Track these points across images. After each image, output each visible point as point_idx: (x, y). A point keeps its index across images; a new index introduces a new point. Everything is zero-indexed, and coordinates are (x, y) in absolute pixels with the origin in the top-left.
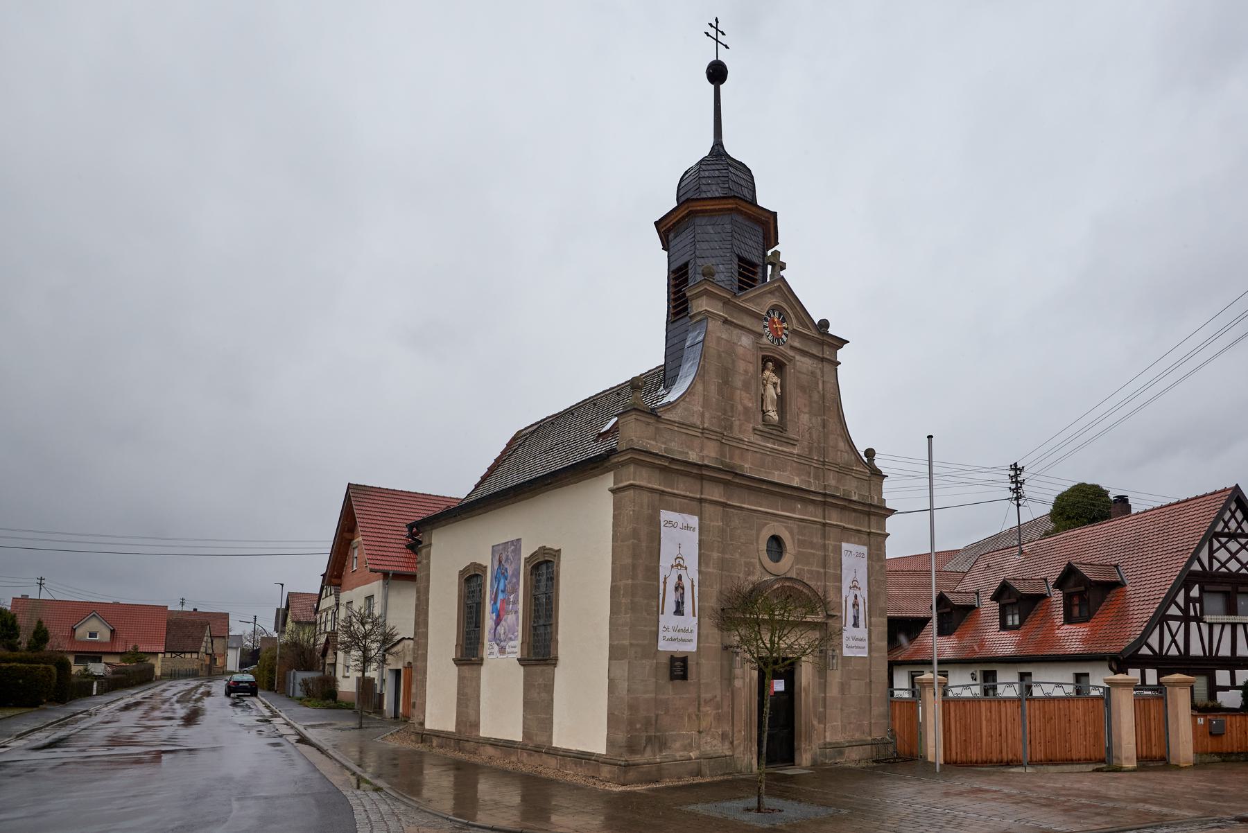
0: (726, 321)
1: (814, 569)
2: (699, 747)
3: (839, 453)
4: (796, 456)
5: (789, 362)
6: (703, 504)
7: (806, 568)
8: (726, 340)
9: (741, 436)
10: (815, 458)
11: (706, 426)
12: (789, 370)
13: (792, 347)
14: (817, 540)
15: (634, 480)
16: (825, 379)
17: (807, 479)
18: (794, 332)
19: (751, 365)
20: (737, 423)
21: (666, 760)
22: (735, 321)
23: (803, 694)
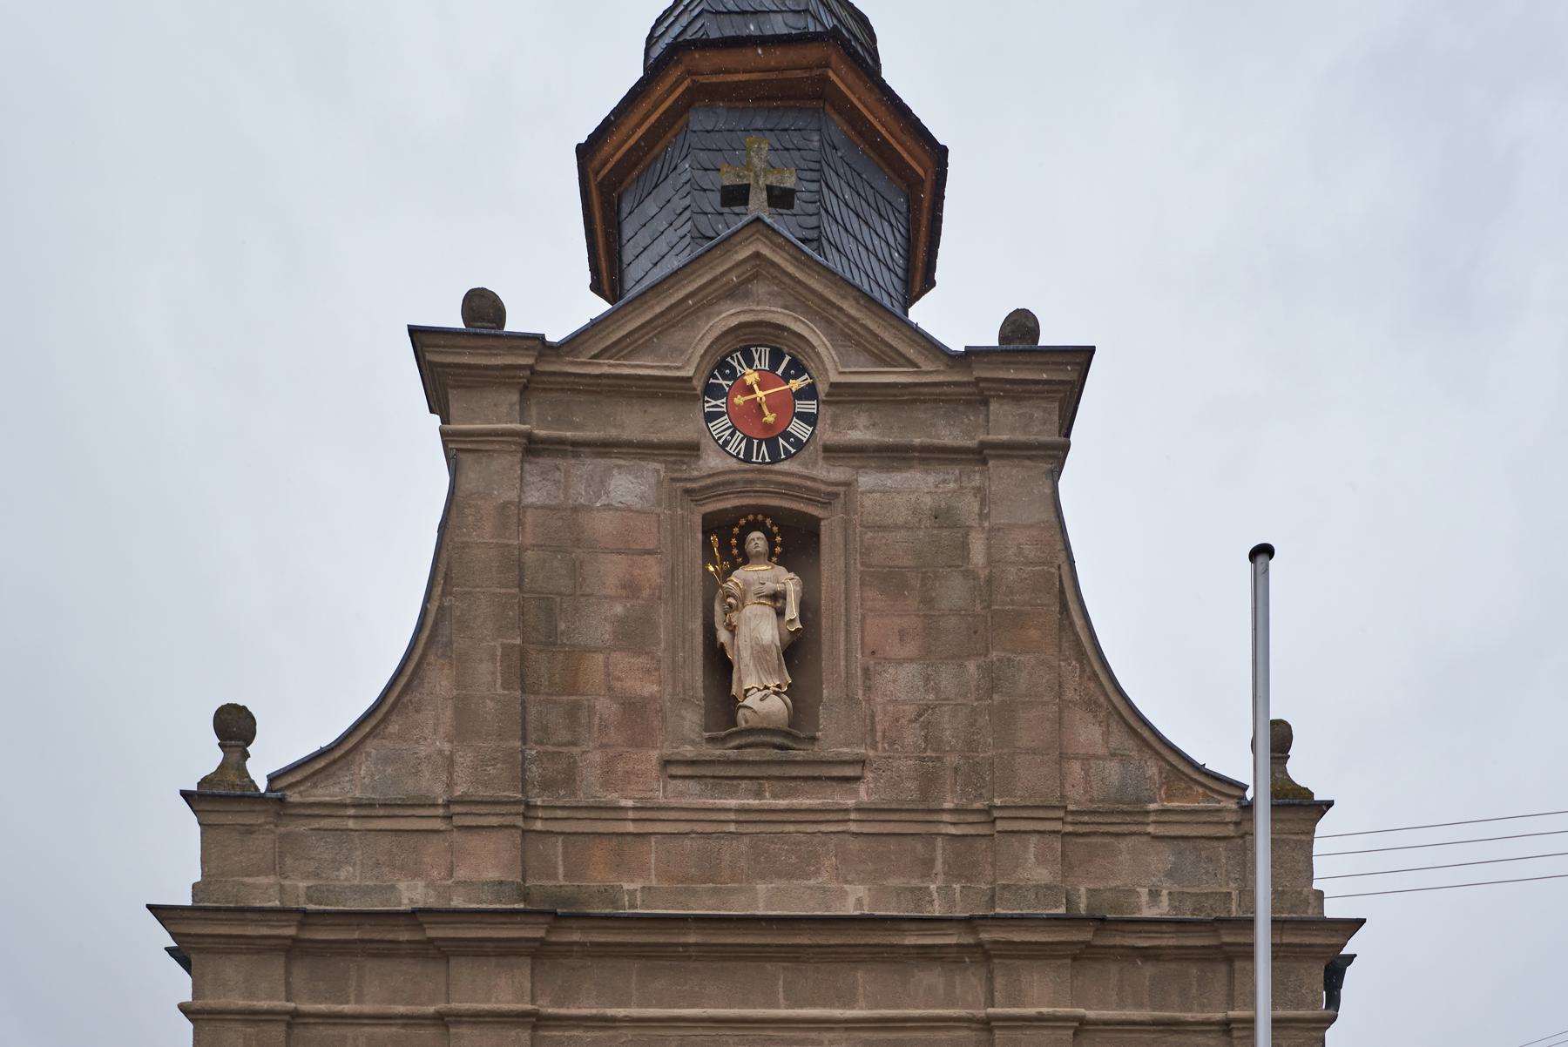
0: (533, 447)
3: (1076, 767)
4: (853, 816)
5: (825, 505)
8: (543, 507)
9: (613, 797)
10: (947, 805)
13: (834, 452)
15: (357, 1002)
16: (999, 517)
17: (915, 882)
18: (846, 396)
19: (651, 560)
20: (596, 757)
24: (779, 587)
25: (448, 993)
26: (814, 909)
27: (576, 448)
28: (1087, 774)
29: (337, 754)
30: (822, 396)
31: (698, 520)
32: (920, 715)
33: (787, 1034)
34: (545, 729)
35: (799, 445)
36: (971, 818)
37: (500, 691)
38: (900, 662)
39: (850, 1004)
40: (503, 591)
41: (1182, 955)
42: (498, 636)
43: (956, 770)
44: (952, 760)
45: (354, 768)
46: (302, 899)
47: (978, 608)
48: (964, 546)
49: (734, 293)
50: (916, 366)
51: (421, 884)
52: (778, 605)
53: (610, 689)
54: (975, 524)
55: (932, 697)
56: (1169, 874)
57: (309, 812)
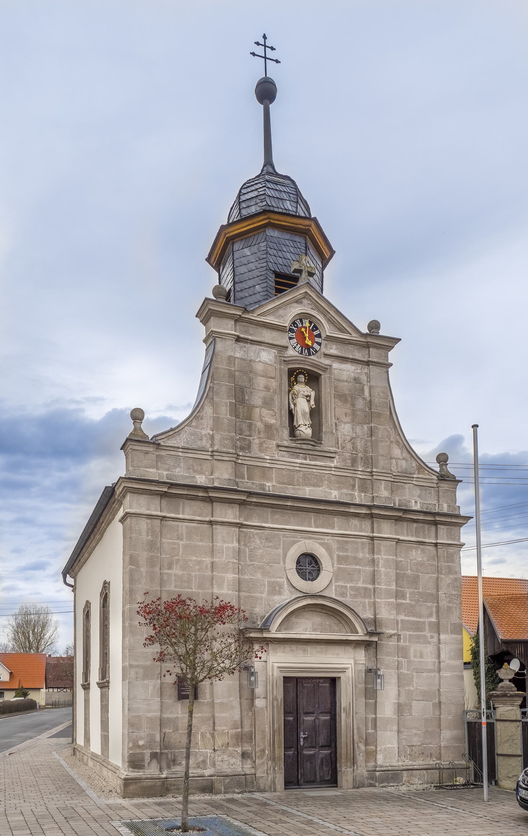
0: (238, 339)
1: (360, 585)
2: (214, 765)
4: (333, 469)
6: (214, 527)
7: (348, 585)
8: (241, 359)
9: (262, 455)
10: (360, 469)
11: (215, 448)
12: (324, 377)
13: (326, 355)
14: (364, 554)
16: (373, 383)
17: (350, 492)
19: (272, 380)
20: (257, 441)
21: (174, 776)
22: (250, 337)
23: (343, 715)
24: (309, 394)
25: (212, 514)
26: (322, 497)
27: (253, 342)
28: (397, 463)
29: (177, 430)
30: (323, 338)
31: (286, 369)
32: (351, 440)
33: (315, 536)
34: (241, 430)
35: (316, 351)
36: (366, 474)
37: (229, 417)
38: (345, 423)
39: (333, 528)
40: (230, 384)
41: (424, 522)
42: (228, 399)
43: (361, 458)
44: (360, 455)
45: (181, 435)
46: (165, 478)
47: (367, 409)
48: (363, 390)
49: (298, 301)
50: (351, 334)
51: (204, 477)
52: (308, 399)
53: (261, 420)
54: (365, 383)
55: (354, 434)
56: (419, 496)
57: (167, 448)
